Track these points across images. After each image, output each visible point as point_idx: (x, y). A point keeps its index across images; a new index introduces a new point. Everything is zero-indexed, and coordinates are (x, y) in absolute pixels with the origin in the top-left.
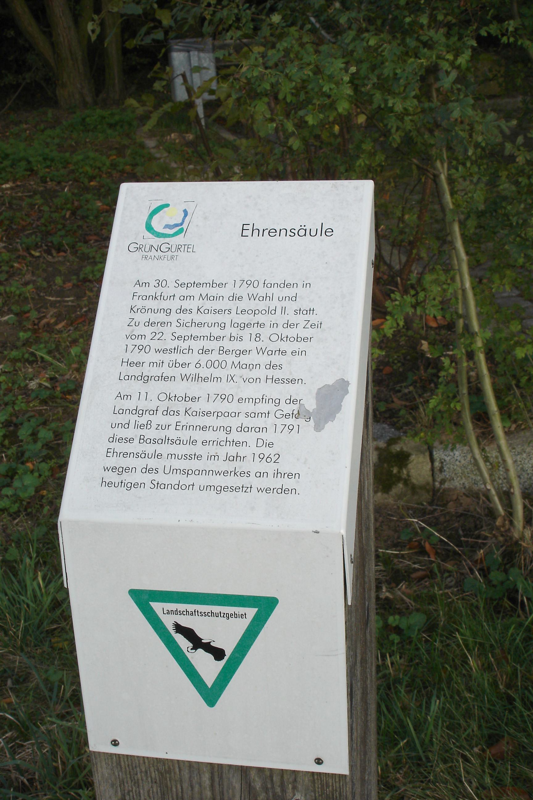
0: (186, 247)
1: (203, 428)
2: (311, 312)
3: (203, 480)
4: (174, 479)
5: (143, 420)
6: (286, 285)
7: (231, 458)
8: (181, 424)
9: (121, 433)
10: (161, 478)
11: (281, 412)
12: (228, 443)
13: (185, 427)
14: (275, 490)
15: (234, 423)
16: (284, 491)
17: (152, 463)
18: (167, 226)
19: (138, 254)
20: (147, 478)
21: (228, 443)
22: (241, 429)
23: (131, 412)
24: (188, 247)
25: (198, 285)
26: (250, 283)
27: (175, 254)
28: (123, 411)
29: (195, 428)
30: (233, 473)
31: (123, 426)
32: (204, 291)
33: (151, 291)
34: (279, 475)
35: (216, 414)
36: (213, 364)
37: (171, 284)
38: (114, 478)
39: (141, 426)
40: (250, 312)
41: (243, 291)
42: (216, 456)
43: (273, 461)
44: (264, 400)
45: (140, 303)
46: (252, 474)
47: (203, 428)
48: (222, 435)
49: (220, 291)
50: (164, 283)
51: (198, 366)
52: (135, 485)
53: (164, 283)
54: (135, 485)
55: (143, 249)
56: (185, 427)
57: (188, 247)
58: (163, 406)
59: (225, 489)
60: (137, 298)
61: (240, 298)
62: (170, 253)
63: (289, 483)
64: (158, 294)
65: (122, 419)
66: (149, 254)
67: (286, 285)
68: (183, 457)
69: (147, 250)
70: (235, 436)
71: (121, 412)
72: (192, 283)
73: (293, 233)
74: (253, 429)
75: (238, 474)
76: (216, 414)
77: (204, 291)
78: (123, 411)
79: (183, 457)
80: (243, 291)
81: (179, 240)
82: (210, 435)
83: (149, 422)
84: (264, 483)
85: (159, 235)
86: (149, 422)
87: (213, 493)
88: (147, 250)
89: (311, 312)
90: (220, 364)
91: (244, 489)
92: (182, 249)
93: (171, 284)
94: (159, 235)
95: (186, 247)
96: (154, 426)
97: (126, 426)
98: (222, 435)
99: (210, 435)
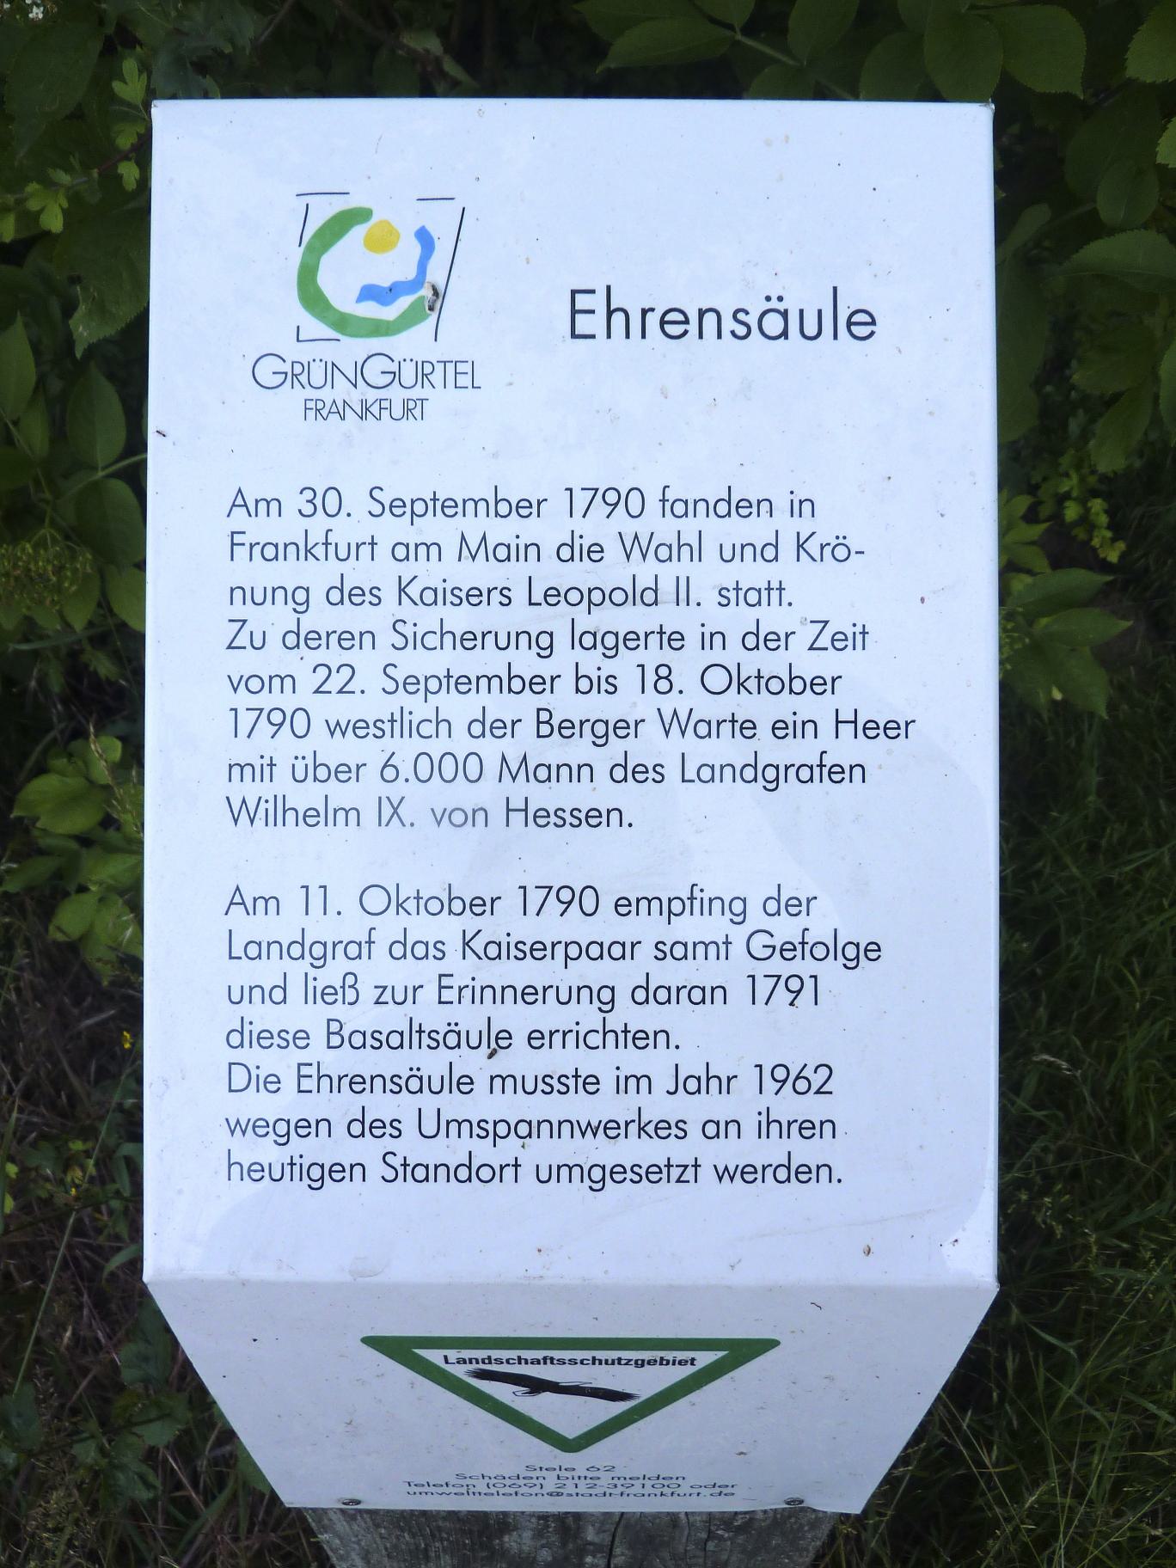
0: (450, 367)
1: (528, 995)
2: (775, 594)
3: (545, 1152)
4: (451, 1151)
5: (332, 974)
6: (740, 507)
7: (692, 1085)
8: (456, 982)
9: (263, 1016)
10: (410, 1147)
11: (762, 939)
12: (611, 1037)
13: (467, 993)
14: (769, 1171)
15: (623, 975)
16: (801, 1173)
17: (381, 1105)
18: (369, 293)
19: (293, 397)
20: (369, 1150)
21: (611, 1037)
22: (647, 993)
23: (285, 951)
24: (461, 373)
25: (447, 507)
26: (616, 500)
27: (417, 393)
28: (258, 950)
29: (499, 994)
30: (633, 1128)
31: (267, 996)
32: (474, 526)
33: (287, 528)
34: (774, 1127)
35: (560, 949)
36: (436, 767)
37: (357, 501)
38: (268, 1152)
39: (327, 995)
40: (574, 597)
41: (598, 527)
42: (623, 1084)
43: (814, 1088)
44: (697, 903)
45: (262, 575)
46: (694, 1130)
47: (528, 995)
48: (587, 1015)
49: (530, 530)
50: (332, 498)
51: (390, 773)
52: (337, 1172)
53: (332, 498)
54: (337, 1172)
55: (303, 378)
56: (467, 993)
57: (461, 373)
58: (389, 928)
59: (616, 1173)
60: (242, 553)
61: (595, 552)
62: (396, 394)
63: (806, 1152)
64: (317, 536)
65: (267, 972)
66: (327, 395)
67: (740, 507)
68: (541, 1086)
69: (317, 379)
70: (627, 1014)
71: (253, 951)
72: (428, 497)
73: (775, 322)
74: (684, 993)
75: (650, 1129)
76: (560, 949)
77: (474, 526)
78: (258, 950)
79: (541, 1086)
80: (598, 527)
81: (413, 344)
82: (548, 1016)
83: (350, 980)
84: (730, 1152)
85: (344, 324)
86: (350, 980)
87: (580, 1189)
88: (317, 379)
89: (775, 594)
90: (461, 767)
91: (675, 1172)
92: (437, 378)
93: (357, 501)
94: (344, 324)
95: (450, 367)
96: (368, 994)
97: (278, 995)
98: (587, 1015)
99: (548, 1016)
